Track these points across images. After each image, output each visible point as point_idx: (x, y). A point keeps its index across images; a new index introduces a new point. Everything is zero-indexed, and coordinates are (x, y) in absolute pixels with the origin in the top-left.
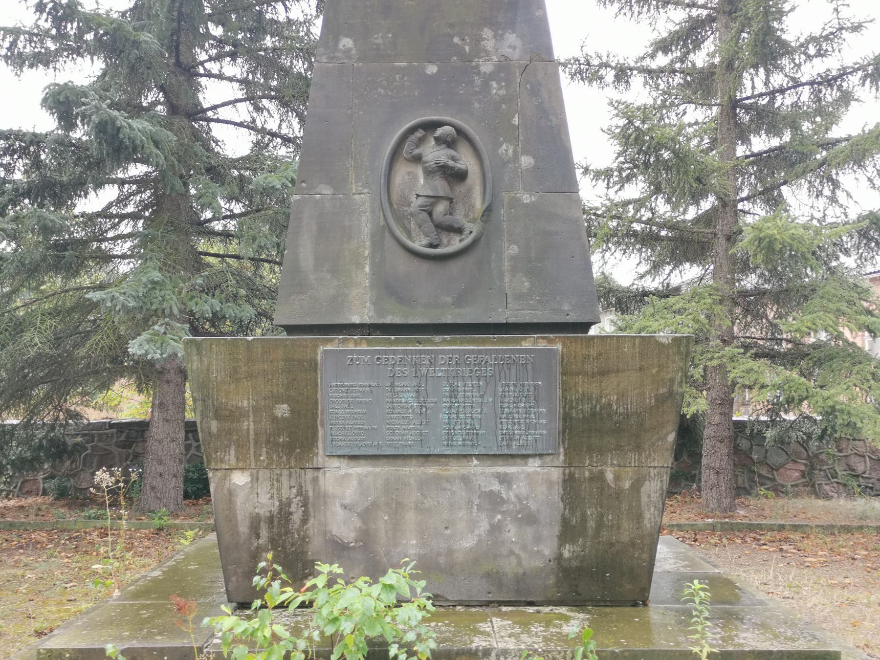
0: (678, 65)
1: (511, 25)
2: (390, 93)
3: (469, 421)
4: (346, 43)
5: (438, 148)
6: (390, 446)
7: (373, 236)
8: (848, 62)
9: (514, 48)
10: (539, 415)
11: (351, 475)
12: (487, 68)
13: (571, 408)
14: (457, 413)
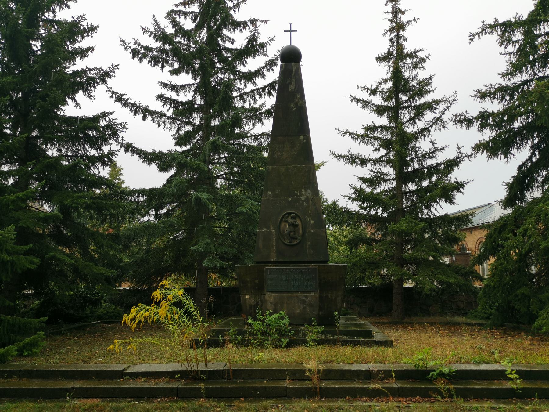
4: (269, 193)
8: (438, 162)
12: (303, 199)
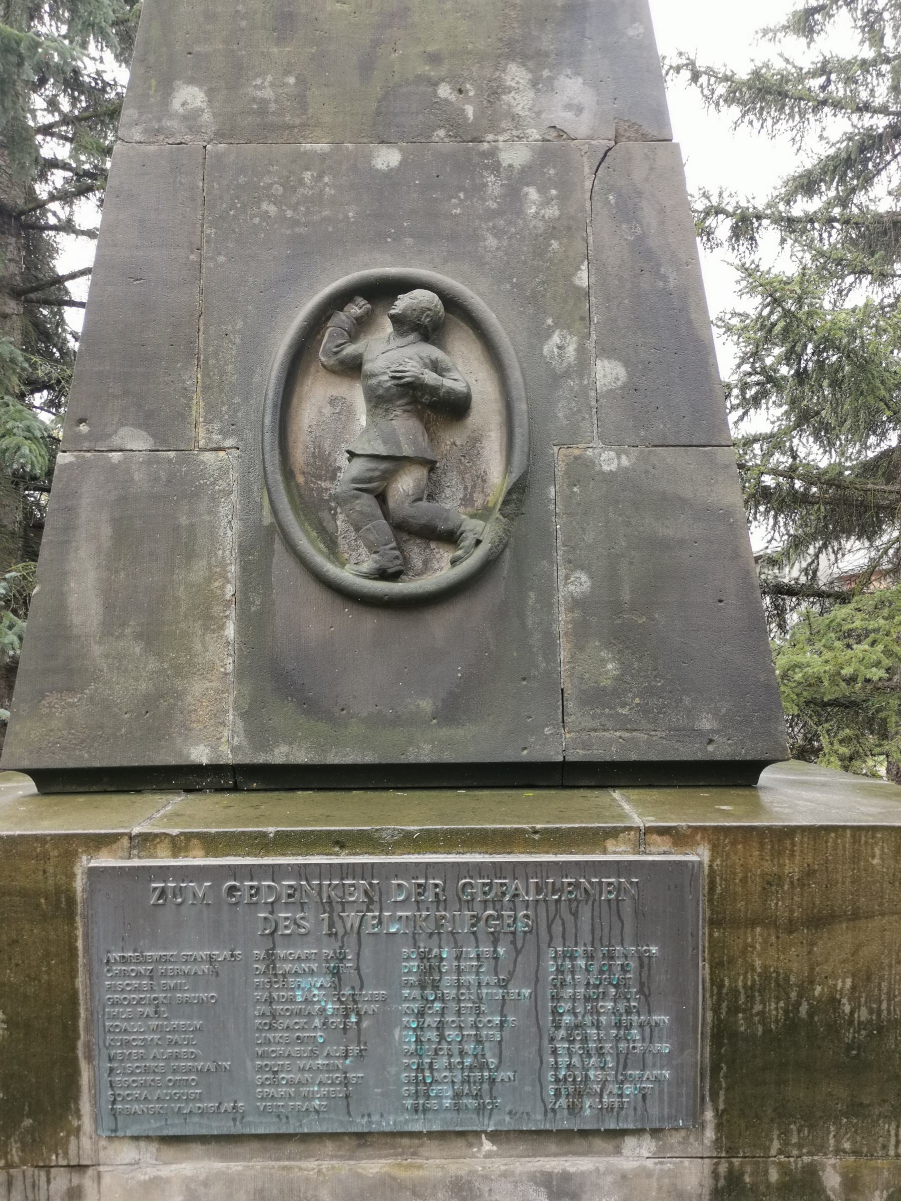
0: (836, 211)
1: (570, 57)
2: (289, 213)
3: (470, 1047)
4: (190, 96)
6: (264, 1112)
7: (244, 550)
10: (651, 1032)
12: (515, 156)
13: (734, 1009)
14: (441, 1027)
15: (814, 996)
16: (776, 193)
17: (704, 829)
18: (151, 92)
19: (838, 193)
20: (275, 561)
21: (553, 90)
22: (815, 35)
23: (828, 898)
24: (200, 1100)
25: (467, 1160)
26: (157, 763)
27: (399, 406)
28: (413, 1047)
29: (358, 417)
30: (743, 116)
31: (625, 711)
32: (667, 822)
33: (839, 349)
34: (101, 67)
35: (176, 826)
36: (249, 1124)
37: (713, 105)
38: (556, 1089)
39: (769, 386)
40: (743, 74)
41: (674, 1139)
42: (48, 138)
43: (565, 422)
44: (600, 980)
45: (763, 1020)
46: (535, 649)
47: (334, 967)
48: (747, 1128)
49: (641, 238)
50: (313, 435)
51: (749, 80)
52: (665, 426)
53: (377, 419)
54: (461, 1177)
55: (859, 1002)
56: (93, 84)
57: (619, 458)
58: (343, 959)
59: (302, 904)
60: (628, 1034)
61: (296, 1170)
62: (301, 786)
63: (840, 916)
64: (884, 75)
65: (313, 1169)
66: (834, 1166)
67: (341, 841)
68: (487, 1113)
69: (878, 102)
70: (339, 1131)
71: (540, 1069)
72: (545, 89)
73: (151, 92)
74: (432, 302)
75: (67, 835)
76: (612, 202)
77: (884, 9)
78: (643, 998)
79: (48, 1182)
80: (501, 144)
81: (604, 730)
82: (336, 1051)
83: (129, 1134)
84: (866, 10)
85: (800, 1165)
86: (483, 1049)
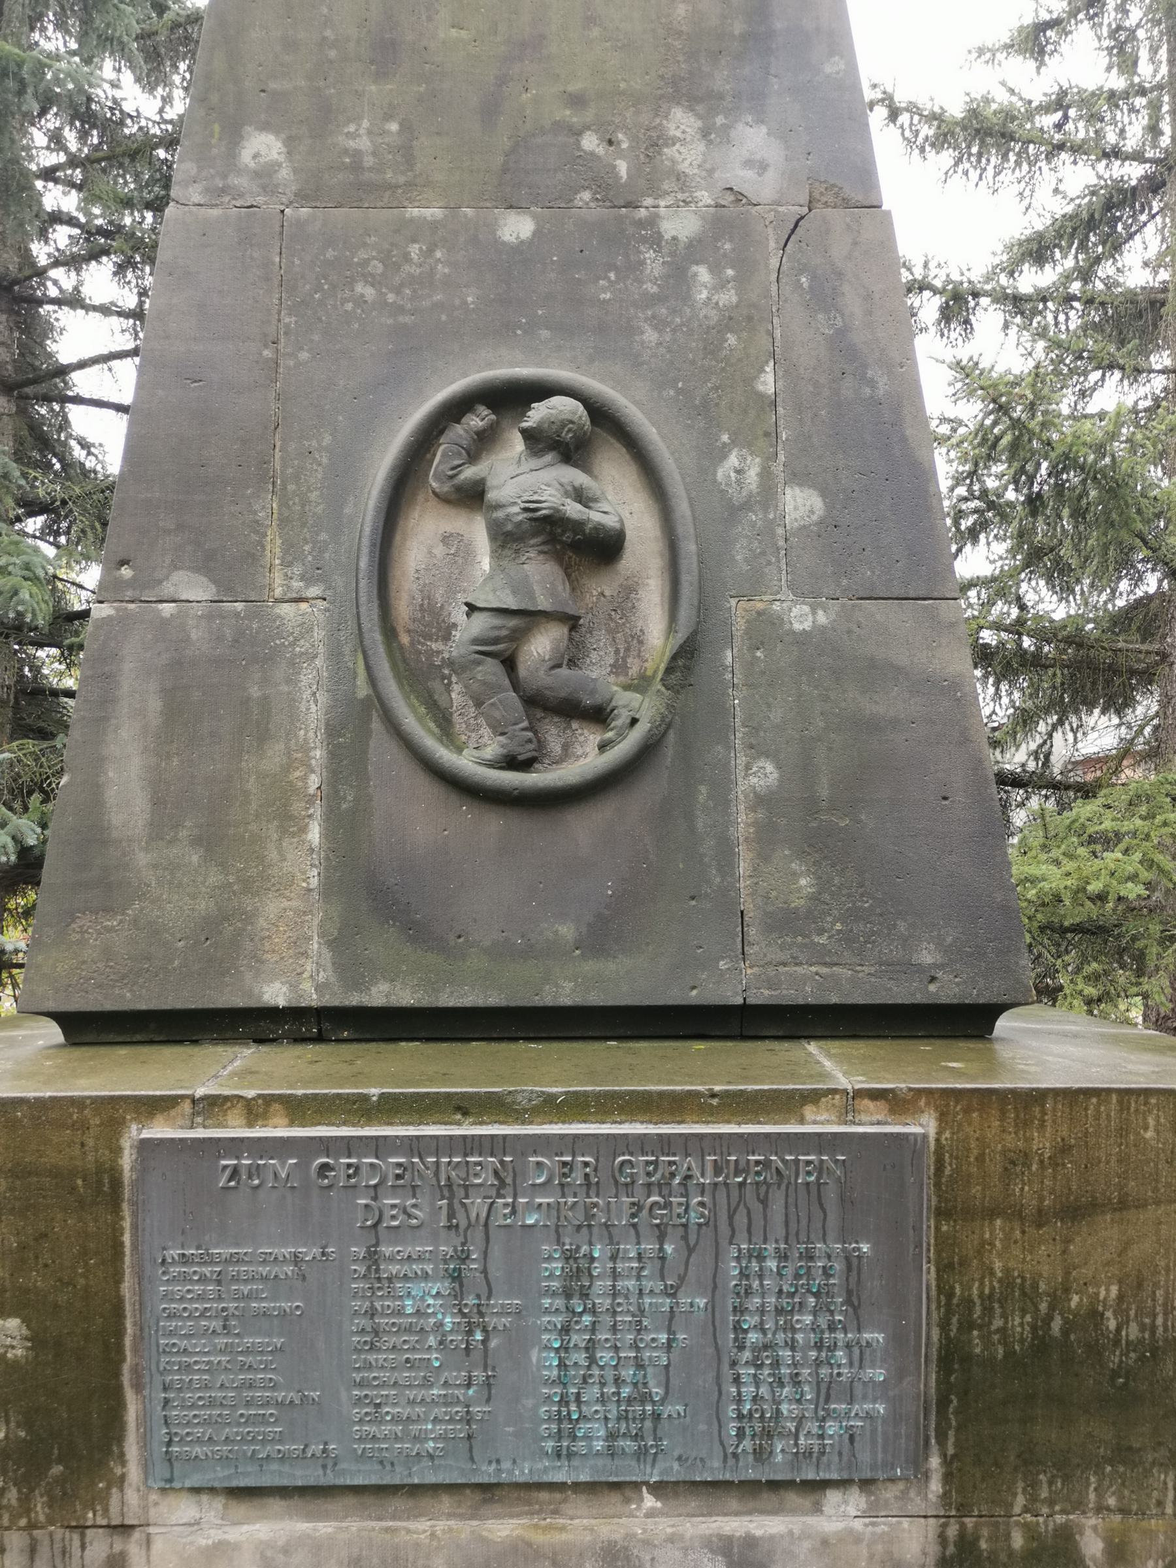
0: (1076, 287)
1: (752, 101)
2: (391, 298)
3: (628, 1373)
4: (263, 146)
5: (535, 463)
6: (363, 1457)
7: (332, 731)
9: (762, 167)
10: (861, 1354)
11: (236, 1547)
12: (680, 225)
14: (591, 1347)
15: (1069, 1307)
16: (997, 261)
17: (930, 1092)
18: (214, 141)
19: (1077, 262)
20: (372, 743)
21: (729, 142)
22: (1047, 58)
23: (1088, 1183)
24: (280, 1442)
25: (624, 1520)
26: (220, 1006)
27: (533, 546)
28: (555, 1372)
29: (478, 559)
30: (956, 164)
31: (822, 940)
32: (881, 1082)
33: (1082, 468)
34: (118, 94)
35: (251, 1086)
36: (344, 1472)
37: (917, 151)
38: (739, 1428)
39: (990, 514)
40: (956, 110)
41: (890, 1493)
42: (51, 185)
43: (746, 568)
44: (796, 1286)
45: (1005, 1338)
46: (706, 860)
47: (454, 1270)
48: (983, 1479)
49: (842, 332)
50: (421, 582)
51: (963, 119)
52: (873, 572)
53: (505, 563)
54: (616, 1542)
55: (1128, 1316)
56: (108, 115)
57: (814, 613)
58: (465, 1258)
59: (414, 1187)
60: (832, 1357)
61: (403, 1533)
62: (405, 1035)
63: (1104, 1205)
64: (1138, 111)
65: (425, 1531)
66: (1095, 1528)
67: (463, 1107)
68: (650, 1459)
69: (1130, 145)
70: (459, 1481)
71: (718, 1402)
72: (718, 140)
73: (214, 141)
74: (575, 413)
75: (112, 1098)
76: (805, 285)
77: (1138, 26)
78: (850, 1310)
79: (83, 1547)
80: (662, 211)
81: (796, 964)
82: (456, 1378)
83: (188, 1484)
84: (1114, 26)
85: (1051, 1526)
86: (645, 1376)
